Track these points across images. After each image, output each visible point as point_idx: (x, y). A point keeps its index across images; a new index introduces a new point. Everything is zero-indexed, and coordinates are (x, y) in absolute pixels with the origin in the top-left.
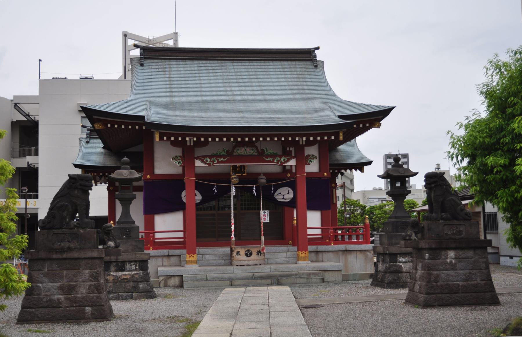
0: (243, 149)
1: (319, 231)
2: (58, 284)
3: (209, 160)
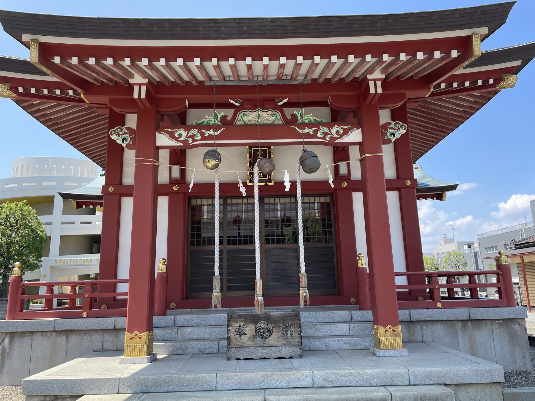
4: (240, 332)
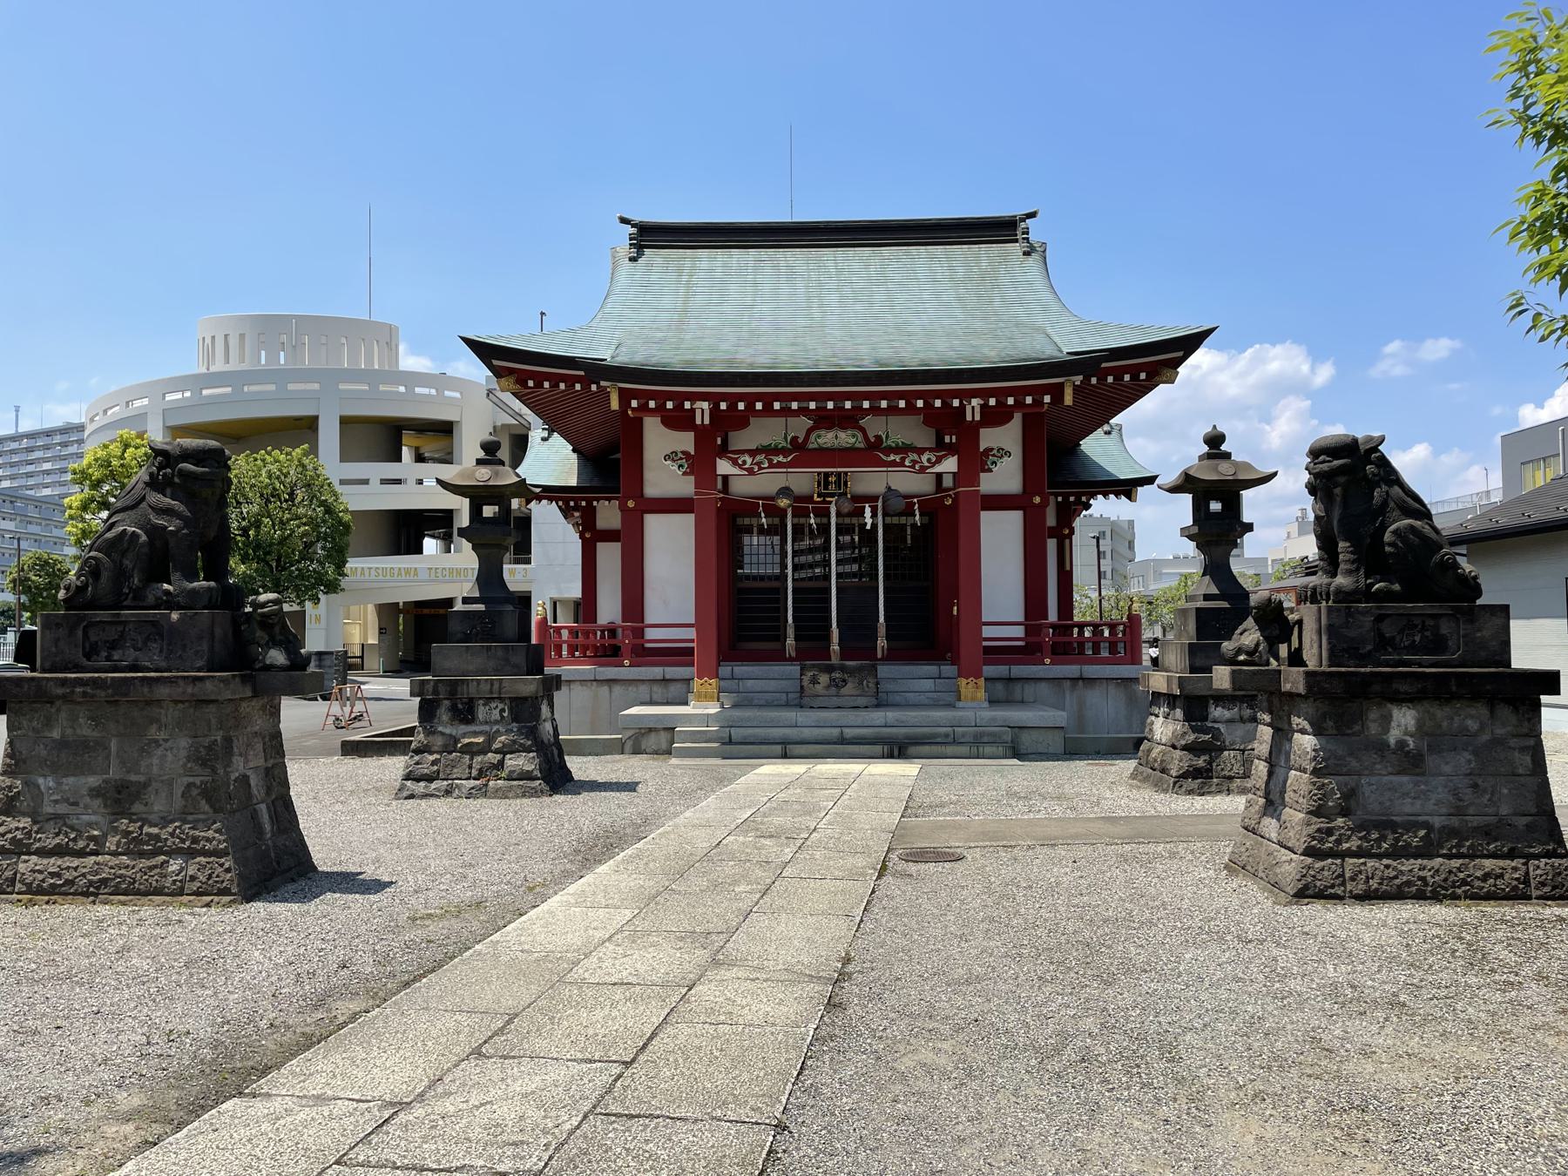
0: (831, 435)
1: (1019, 632)
2: (93, 781)
3: (749, 460)
4: (814, 681)
